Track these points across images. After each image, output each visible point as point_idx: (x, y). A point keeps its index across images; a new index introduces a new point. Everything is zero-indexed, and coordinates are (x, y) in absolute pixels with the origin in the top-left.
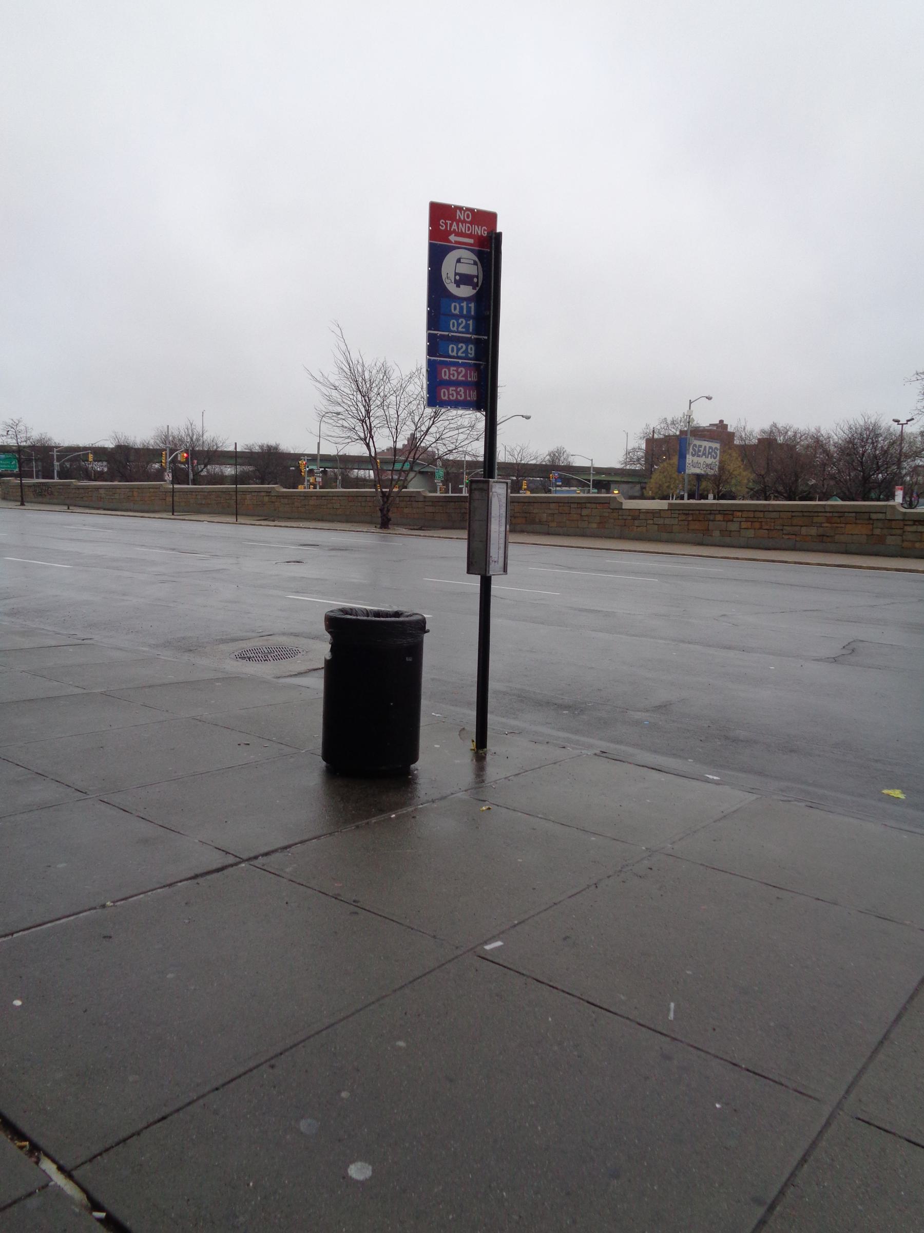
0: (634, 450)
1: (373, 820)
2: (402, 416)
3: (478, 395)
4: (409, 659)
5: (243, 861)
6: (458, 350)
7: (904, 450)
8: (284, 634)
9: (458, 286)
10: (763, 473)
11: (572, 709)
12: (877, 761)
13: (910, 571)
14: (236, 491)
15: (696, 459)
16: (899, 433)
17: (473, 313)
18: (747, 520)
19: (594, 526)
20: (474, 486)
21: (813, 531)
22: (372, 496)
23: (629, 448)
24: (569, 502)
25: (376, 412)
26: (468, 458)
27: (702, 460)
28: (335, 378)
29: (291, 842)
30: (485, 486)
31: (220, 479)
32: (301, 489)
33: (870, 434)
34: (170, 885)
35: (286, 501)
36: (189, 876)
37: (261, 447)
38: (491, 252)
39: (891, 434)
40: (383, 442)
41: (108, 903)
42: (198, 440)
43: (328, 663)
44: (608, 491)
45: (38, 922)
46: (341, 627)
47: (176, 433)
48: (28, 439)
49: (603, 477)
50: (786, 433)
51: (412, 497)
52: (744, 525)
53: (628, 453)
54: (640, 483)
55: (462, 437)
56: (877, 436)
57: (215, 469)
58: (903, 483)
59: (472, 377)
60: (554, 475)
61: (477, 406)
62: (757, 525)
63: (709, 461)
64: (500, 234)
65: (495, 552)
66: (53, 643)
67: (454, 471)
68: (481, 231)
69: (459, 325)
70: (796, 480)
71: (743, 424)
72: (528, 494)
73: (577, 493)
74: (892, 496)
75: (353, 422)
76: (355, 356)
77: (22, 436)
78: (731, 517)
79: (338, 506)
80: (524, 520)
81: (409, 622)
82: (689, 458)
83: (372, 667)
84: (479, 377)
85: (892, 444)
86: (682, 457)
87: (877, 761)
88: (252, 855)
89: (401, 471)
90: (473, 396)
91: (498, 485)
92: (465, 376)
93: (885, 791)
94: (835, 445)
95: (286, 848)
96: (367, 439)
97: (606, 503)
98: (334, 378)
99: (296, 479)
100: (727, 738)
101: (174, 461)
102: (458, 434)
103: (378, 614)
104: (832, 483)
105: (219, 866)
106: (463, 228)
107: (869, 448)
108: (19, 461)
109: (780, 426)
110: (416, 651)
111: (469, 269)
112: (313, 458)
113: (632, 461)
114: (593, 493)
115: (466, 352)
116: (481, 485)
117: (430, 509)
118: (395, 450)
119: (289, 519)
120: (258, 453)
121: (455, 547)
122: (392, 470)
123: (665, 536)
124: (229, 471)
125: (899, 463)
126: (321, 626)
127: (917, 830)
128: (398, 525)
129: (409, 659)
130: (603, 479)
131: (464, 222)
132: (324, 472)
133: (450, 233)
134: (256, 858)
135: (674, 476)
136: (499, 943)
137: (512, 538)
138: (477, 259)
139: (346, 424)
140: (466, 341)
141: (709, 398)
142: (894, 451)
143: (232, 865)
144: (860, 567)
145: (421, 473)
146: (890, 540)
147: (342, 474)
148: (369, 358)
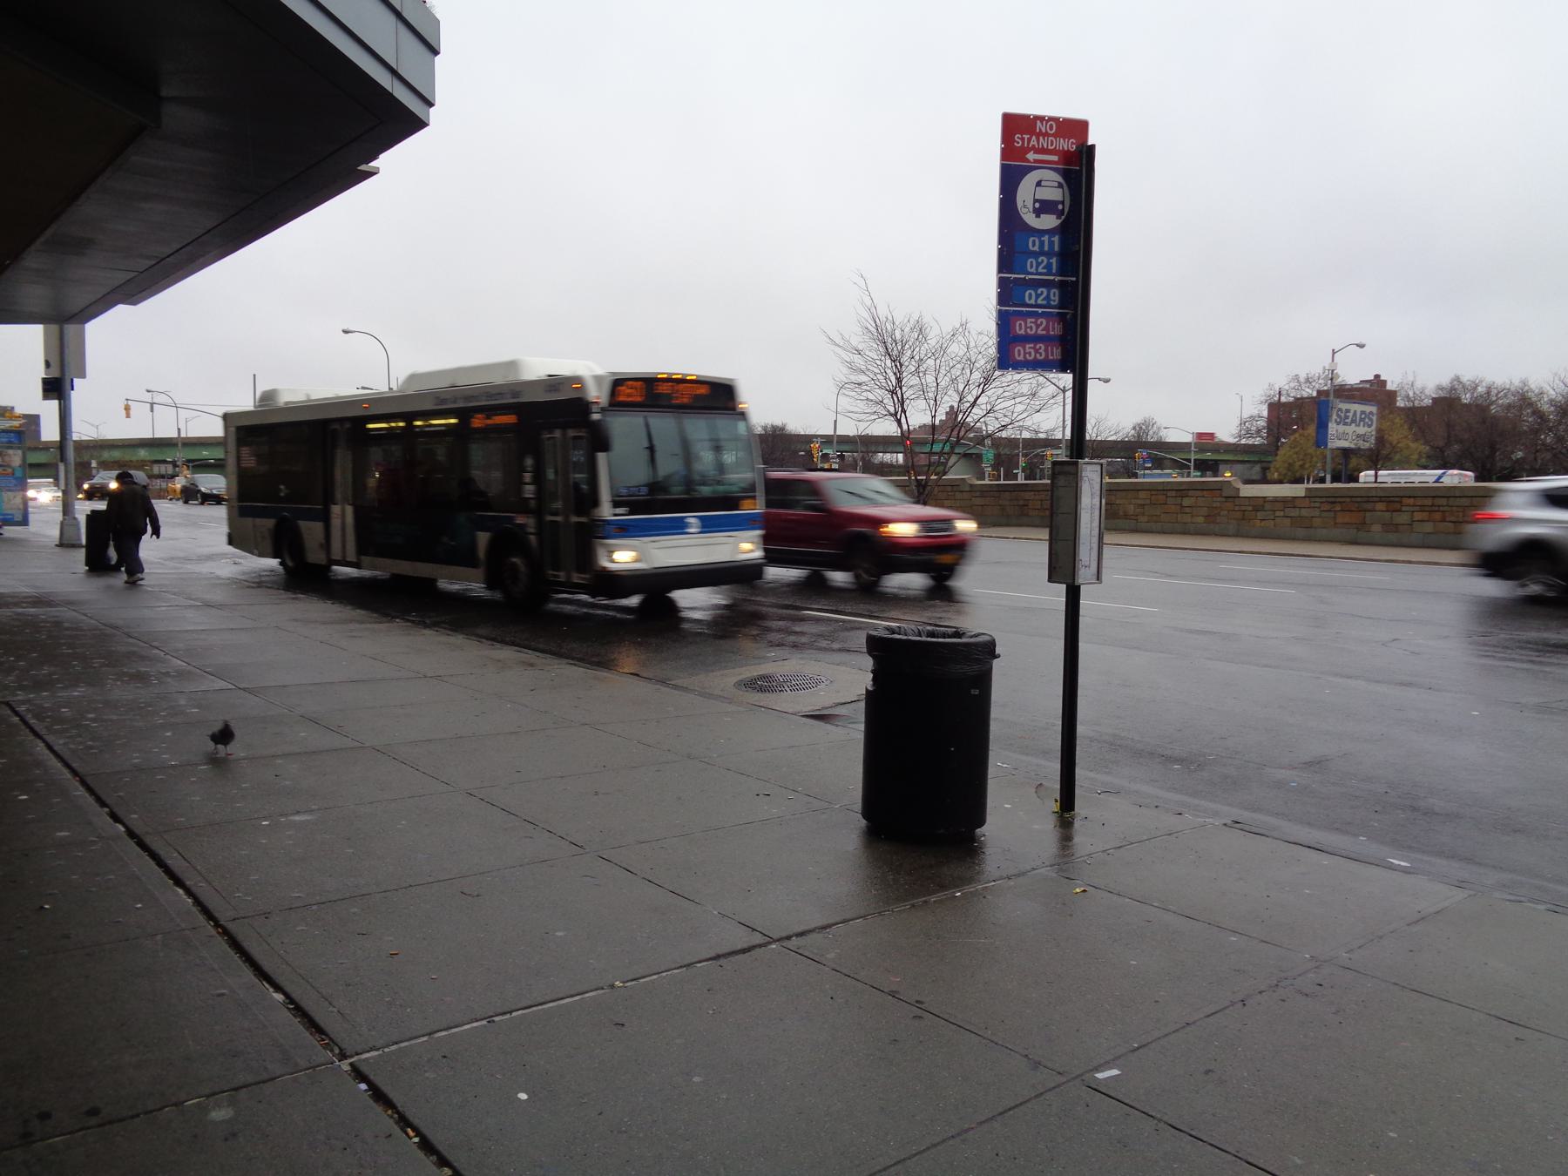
0: (1252, 418)
2: (943, 384)
3: (1063, 353)
4: (976, 692)
6: (1038, 296)
9: (1038, 216)
10: (1441, 444)
11: (1186, 763)
15: (1341, 428)
17: (1056, 248)
18: (1422, 508)
19: (1201, 519)
20: (1058, 468)
23: (1245, 416)
24: (1164, 489)
25: (910, 380)
26: (1026, 435)
27: (1351, 429)
29: (831, 921)
37: (765, 428)
40: (918, 417)
43: (872, 698)
44: (1216, 473)
50: (1475, 388)
52: (1418, 516)
53: (1242, 423)
54: (1260, 462)
59: (1056, 329)
62: (1438, 516)
63: (1362, 430)
64: (1093, 147)
65: (1086, 553)
68: (1068, 145)
69: (1038, 264)
71: (1411, 379)
73: (1173, 477)
76: (882, 312)
78: (1397, 506)
80: (1116, 518)
82: (1333, 428)
86: (1323, 426)
88: (784, 934)
89: (941, 453)
90: (1056, 353)
91: (1089, 468)
94: (1551, 401)
97: (1218, 489)
100: (1414, 809)
102: (1033, 407)
104: (1548, 456)
105: (745, 946)
106: (1044, 142)
109: (1464, 379)
110: (983, 681)
111: (1053, 194)
112: (827, 440)
114: (1195, 477)
115: (1047, 298)
116: (1067, 468)
119: (325, 423)
121: (1033, 549)
122: (931, 453)
123: (1301, 532)
129: (976, 692)
130: (1207, 455)
131: (1046, 135)
132: (841, 457)
133: (1028, 150)
134: (789, 938)
135: (1311, 451)
136: (1115, 1072)
138: (1061, 180)
139: (871, 396)
140: (1047, 284)
141: (1361, 346)
143: (760, 946)
145: (965, 455)
147: (863, 459)
148: (900, 311)
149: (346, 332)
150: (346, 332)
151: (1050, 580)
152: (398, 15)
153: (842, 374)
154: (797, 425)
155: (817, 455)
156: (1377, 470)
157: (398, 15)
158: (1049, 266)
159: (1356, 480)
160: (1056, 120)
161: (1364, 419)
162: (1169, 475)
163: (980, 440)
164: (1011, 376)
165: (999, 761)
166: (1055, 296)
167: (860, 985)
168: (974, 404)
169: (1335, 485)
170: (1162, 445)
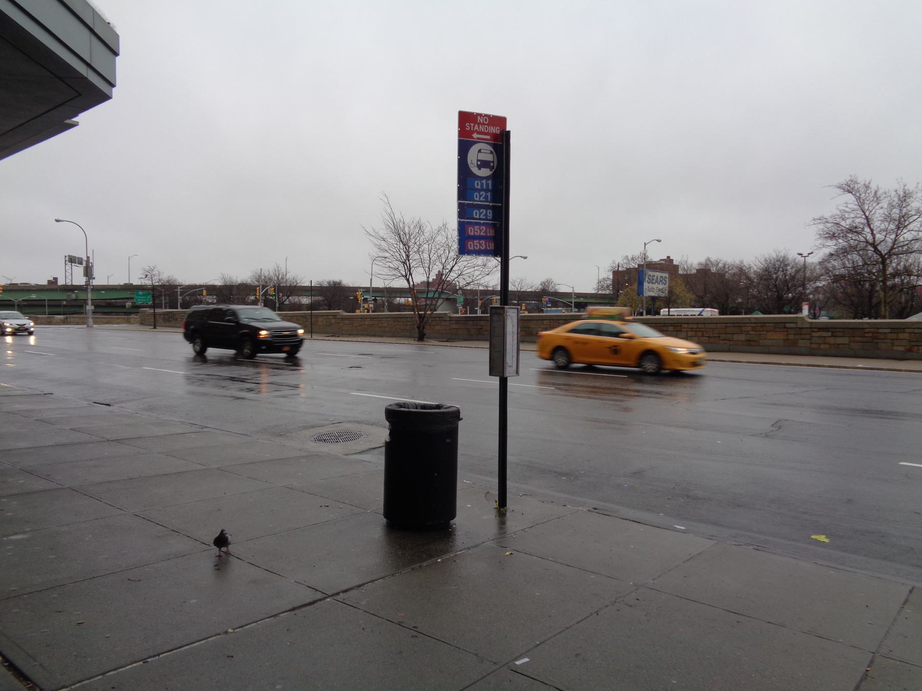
1: (425, 564)
4: (448, 441)
5: (329, 596)
6: (480, 214)
7: (807, 275)
8: (350, 422)
10: (701, 294)
12: (804, 513)
13: (818, 366)
14: (311, 315)
15: (651, 285)
16: (802, 263)
20: (494, 311)
21: (742, 337)
22: (411, 317)
23: (601, 278)
25: (414, 256)
26: (481, 288)
27: (655, 286)
28: (383, 233)
30: (501, 311)
31: (299, 307)
32: (358, 313)
33: (782, 263)
34: (275, 616)
35: (347, 322)
36: (288, 608)
37: (329, 283)
38: (502, 145)
39: (796, 264)
40: (419, 277)
41: (230, 630)
42: (282, 278)
43: (388, 445)
45: (178, 645)
46: (399, 418)
47: (266, 274)
48: (160, 280)
49: (582, 300)
51: (441, 317)
53: (599, 282)
55: (477, 273)
56: (786, 265)
57: (294, 299)
58: (808, 300)
59: (491, 233)
60: (545, 299)
61: (495, 254)
62: (700, 334)
63: (661, 286)
64: (509, 132)
65: (510, 359)
66: (181, 431)
67: (472, 298)
68: (495, 130)
70: (727, 300)
72: (526, 314)
74: (800, 310)
75: (397, 264)
76: (398, 217)
77: (156, 279)
78: (679, 328)
79: (385, 325)
81: (448, 413)
82: (646, 285)
83: (420, 448)
84: (496, 232)
85: (797, 271)
86: (641, 284)
87: (804, 513)
89: (433, 298)
90: (491, 246)
91: (511, 310)
92: (486, 232)
93: (813, 537)
95: (360, 586)
96: (407, 277)
98: (383, 233)
99: (353, 305)
100: (688, 497)
101: (265, 294)
102: (481, 273)
103: (424, 407)
104: (754, 301)
105: (311, 600)
106: (482, 128)
107: (780, 274)
108: (153, 297)
109: (712, 260)
110: (453, 434)
111: (489, 157)
112: (366, 290)
113: (603, 288)
115: (486, 215)
117: (454, 326)
118: (428, 284)
119: (350, 335)
120: (326, 287)
122: (427, 298)
124: (305, 300)
125: (804, 285)
126: (382, 416)
127: (842, 567)
128: (430, 338)
129: (448, 441)
132: (375, 300)
133: (474, 132)
134: (338, 594)
136: (526, 660)
137: (522, 347)
139: (391, 265)
141: (659, 241)
142: (800, 276)
143: (320, 600)
144: (780, 364)
145: (447, 299)
146: (801, 343)
147: (388, 301)
148: (408, 216)
149: (57, 221)
150: (57, 221)
151: (491, 374)
152: (91, 30)
153: (375, 252)
154: (349, 281)
155: (361, 299)
156: (669, 308)
157: (91, 30)
158: (486, 197)
159: (659, 314)
160: (488, 116)
161: (662, 280)
162: (561, 311)
163: (456, 291)
164: (465, 258)
165: (464, 480)
166: (490, 214)
167: (380, 620)
168: (450, 271)
169: (649, 317)
170: (557, 294)
